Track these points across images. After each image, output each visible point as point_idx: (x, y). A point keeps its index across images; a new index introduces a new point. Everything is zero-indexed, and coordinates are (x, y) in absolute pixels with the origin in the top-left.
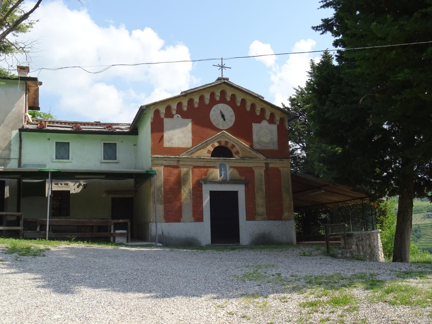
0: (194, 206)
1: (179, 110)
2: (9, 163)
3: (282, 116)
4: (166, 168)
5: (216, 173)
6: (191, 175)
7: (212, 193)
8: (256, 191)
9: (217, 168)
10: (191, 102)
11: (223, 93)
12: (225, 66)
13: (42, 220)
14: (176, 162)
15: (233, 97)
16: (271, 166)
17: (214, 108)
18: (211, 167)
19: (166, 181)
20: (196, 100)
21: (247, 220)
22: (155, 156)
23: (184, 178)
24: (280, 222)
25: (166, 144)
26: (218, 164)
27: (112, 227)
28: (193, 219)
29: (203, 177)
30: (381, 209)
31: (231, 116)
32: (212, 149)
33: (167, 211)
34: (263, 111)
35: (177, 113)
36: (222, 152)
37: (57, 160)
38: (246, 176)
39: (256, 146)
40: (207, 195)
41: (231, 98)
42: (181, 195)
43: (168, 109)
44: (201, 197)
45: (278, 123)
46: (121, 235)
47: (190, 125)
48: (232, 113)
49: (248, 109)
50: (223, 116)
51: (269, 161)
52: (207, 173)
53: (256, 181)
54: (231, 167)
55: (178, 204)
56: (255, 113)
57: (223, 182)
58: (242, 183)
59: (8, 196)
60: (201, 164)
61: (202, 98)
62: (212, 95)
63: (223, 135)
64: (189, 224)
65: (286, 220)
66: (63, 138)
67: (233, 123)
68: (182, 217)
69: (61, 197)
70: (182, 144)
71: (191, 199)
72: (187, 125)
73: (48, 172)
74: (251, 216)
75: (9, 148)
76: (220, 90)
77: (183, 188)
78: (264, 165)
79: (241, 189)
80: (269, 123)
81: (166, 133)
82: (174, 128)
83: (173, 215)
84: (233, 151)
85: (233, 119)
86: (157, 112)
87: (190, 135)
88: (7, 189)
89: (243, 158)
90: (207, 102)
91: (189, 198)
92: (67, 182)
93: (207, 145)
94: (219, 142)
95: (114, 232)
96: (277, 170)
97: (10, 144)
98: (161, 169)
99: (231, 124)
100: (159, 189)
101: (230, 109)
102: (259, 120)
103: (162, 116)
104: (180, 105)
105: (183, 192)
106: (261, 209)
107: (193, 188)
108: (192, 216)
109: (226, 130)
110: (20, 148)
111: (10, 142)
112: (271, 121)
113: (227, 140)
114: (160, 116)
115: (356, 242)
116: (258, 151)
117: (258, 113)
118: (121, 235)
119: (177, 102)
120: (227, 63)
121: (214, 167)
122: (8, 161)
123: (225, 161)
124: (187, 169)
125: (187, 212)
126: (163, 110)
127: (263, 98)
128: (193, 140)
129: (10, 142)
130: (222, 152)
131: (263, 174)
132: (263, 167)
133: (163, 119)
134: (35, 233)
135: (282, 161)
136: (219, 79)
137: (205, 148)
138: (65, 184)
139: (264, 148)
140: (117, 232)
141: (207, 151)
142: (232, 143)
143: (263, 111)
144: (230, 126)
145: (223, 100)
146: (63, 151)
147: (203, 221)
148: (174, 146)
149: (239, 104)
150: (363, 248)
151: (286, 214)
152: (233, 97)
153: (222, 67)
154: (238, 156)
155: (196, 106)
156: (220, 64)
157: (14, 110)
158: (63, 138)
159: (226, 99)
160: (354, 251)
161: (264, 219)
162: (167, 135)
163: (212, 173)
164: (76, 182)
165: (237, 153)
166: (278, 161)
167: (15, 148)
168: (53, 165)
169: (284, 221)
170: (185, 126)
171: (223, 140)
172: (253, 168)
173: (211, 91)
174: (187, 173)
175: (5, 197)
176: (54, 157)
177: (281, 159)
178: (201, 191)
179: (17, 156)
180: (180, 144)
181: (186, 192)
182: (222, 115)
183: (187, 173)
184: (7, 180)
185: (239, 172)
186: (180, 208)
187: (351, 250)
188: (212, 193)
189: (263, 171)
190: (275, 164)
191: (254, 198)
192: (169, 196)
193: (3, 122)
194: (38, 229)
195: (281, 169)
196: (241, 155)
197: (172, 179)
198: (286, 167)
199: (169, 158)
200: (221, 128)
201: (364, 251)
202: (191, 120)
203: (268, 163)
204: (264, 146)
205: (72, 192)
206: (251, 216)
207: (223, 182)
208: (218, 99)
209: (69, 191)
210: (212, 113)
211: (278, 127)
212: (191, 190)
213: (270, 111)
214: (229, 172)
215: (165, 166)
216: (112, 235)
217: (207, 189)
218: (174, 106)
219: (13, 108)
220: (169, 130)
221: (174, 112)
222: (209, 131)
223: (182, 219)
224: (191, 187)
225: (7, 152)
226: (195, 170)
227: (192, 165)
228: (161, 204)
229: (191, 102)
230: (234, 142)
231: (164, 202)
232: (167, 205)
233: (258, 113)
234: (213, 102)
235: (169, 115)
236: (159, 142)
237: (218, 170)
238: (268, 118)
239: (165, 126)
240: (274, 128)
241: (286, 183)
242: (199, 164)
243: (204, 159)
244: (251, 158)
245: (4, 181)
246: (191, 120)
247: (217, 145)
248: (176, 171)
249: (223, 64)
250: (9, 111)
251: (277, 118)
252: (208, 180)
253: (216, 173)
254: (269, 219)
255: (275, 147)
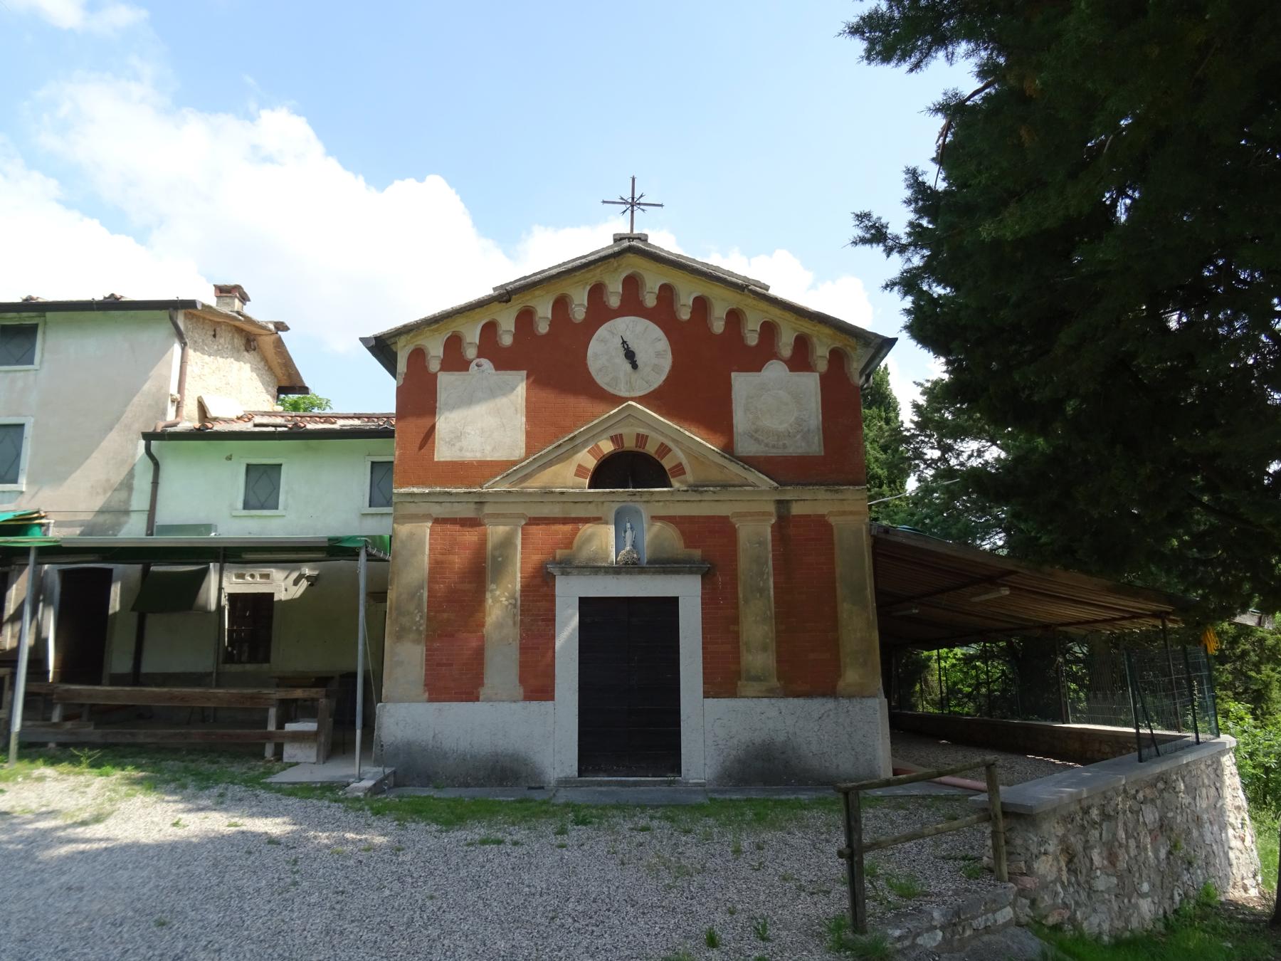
0: (524, 649)
1: (489, 345)
2: (126, 522)
3: (838, 345)
4: (438, 528)
5: (604, 540)
6: (519, 547)
7: (587, 605)
8: (741, 596)
9: (607, 523)
10: (526, 318)
11: (632, 283)
12: (642, 201)
13: (67, 691)
14: (473, 506)
15: (667, 292)
16: (796, 510)
17: (602, 331)
18: (586, 520)
19: (437, 568)
20: (544, 310)
21: (707, 695)
22: (402, 490)
23: (494, 558)
24: (830, 704)
25: (443, 452)
26: (611, 510)
27: (272, 712)
28: (520, 691)
29: (559, 553)
30: (1262, 641)
31: (658, 354)
32: (591, 463)
33: (433, 665)
34: (769, 330)
35: (479, 356)
36: (628, 469)
37: (373, 510)
38: (708, 550)
39: (744, 447)
40: (570, 611)
41: (659, 298)
42: (484, 612)
43: (454, 345)
44: (549, 619)
45: (823, 366)
46: (298, 737)
47: (521, 389)
48: (663, 344)
49: (718, 327)
50: (630, 355)
51: (790, 494)
52: (571, 543)
53: (744, 563)
54: (655, 518)
55: (474, 644)
56: (741, 338)
57: (629, 567)
58: (691, 572)
59: (117, 608)
60: (556, 511)
61: (561, 304)
62: (597, 292)
63: (630, 415)
64: (506, 707)
65: (850, 697)
66: (264, 454)
67: (663, 377)
68: (482, 684)
69: (253, 610)
70: (494, 449)
71: (515, 623)
72: (513, 389)
73: (29, 548)
74: (722, 681)
75: (127, 485)
76: (624, 275)
77: (492, 591)
78: (772, 508)
79: (688, 592)
80: (791, 370)
81: (442, 419)
82: (469, 400)
83: (455, 679)
84: (667, 463)
85: (667, 363)
86: (418, 355)
87: (521, 420)
88: (116, 591)
89: (696, 488)
90: (579, 313)
91: (511, 623)
92: (266, 571)
93: (575, 450)
94: (616, 439)
95: (280, 726)
96: (820, 526)
97: (131, 474)
98: (425, 530)
99: (658, 380)
100: (413, 595)
101: (656, 332)
102: (755, 360)
103: (434, 366)
104: (490, 329)
105: (490, 601)
106: (758, 656)
107: (526, 589)
108: (517, 682)
109: (640, 400)
110: (155, 483)
111: (133, 469)
112: (800, 360)
113: (642, 431)
114: (425, 368)
115: (1063, 840)
116: (750, 462)
117: (752, 340)
118: (298, 737)
119: (484, 322)
120: (648, 192)
121: (597, 520)
122: (123, 519)
123: (638, 498)
124: (507, 528)
125: (502, 667)
126: (435, 350)
127: (767, 288)
128: (528, 434)
129: (133, 469)
130: (628, 469)
131: (769, 537)
132: (770, 514)
133: (435, 376)
134: (43, 730)
135: (837, 491)
136: (618, 239)
137: (568, 458)
138: (262, 576)
139: (773, 452)
140: (290, 727)
141: (573, 469)
142: (662, 439)
143: (769, 330)
144: (656, 386)
145: (632, 305)
146: (262, 486)
147: (552, 699)
148: (469, 456)
149: (685, 315)
150: (1112, 858)
151: (851, 676)
152: (667, 292)
153: (633, 204)
154: (681, 482)
155: (543, 328)
156: (628, 196)
157: (146, 387)
158: (264, 454)
159: (641, 303)
160: (1045, 886)
161: (771, 694)
162: (445, 423)
163: (589, 539)
164: (293, 570)
165: (679, 470)
166: (821, 493)
167: (143, 483)
168: (235, 524)
169: (844, 702)
170: (504, 395)
171: (629, 433)
172: (733, 520)
173: (593, 282)
174: (507, 543)
175: (111, 612)
176: (240, 504)
177: (834, 484)
178: (551, 598)
179: (146, 506)
180: (488, 448)
181: (500, 603)
182: (633, 356)
183: (507, 543)
184: (118, 568)
185: (683, 533)
186: (479, 656)
187: (1029, 882)
188: (587, 605)
189: (769, 530)
190: (811, 503)
191: (735, 620)
192: (445, 615)
193: (118, 419)
194: (56, 716)
195: (832, 520)
196: (690, 477)
197: (459, 561)
198: (852, 513)
199: (449, 494)
200: (624, 394)
201: (1122, 865)
202: (524, 373)
203: (788, 501)
204: (773, 446)
205: (280, 596)
206: (722, 681)
207: (629, 567)
208: (614, 302)
209: (272, 595)
210: (594, 347)
211: (823, 378)
212: (518, 595)
213: (795, 330)
214: (652, 534)
215: (437, 521)
216: (269, 736)
217: (569, 594)
218: (472, 335)
219: (145, 381)
220: (453, 407)
221: (471, 353)
222: (583, 404)
223: (483, 692)
224: (518, 587)
225: (123, 495)
226: (536, 530)
227: (523, 516)
228: (417, 642)
229: (526, 318)
230: (666, 436)
231: (427, 636)
232: (437, 645)
233: (752, 340)
234: (599, 312)
235: (455, 360)
236: (421, 448)
237: (612, 528)
238: (787, 352)
239: (442, 396)
240: (810, 383)
241: (854, 568)
242: (546, 511)
243: (562, 493)
244: (725, 486)
245: (111, 571)
246: (524, 373)
247: (607, 447)
248: (470, 536)
249: (637, 196)
250: (133, 392)
251: (821, 352)
252: (576, 563)
253: (604, 540)
254: (789, 692)
255: (815, 447)
